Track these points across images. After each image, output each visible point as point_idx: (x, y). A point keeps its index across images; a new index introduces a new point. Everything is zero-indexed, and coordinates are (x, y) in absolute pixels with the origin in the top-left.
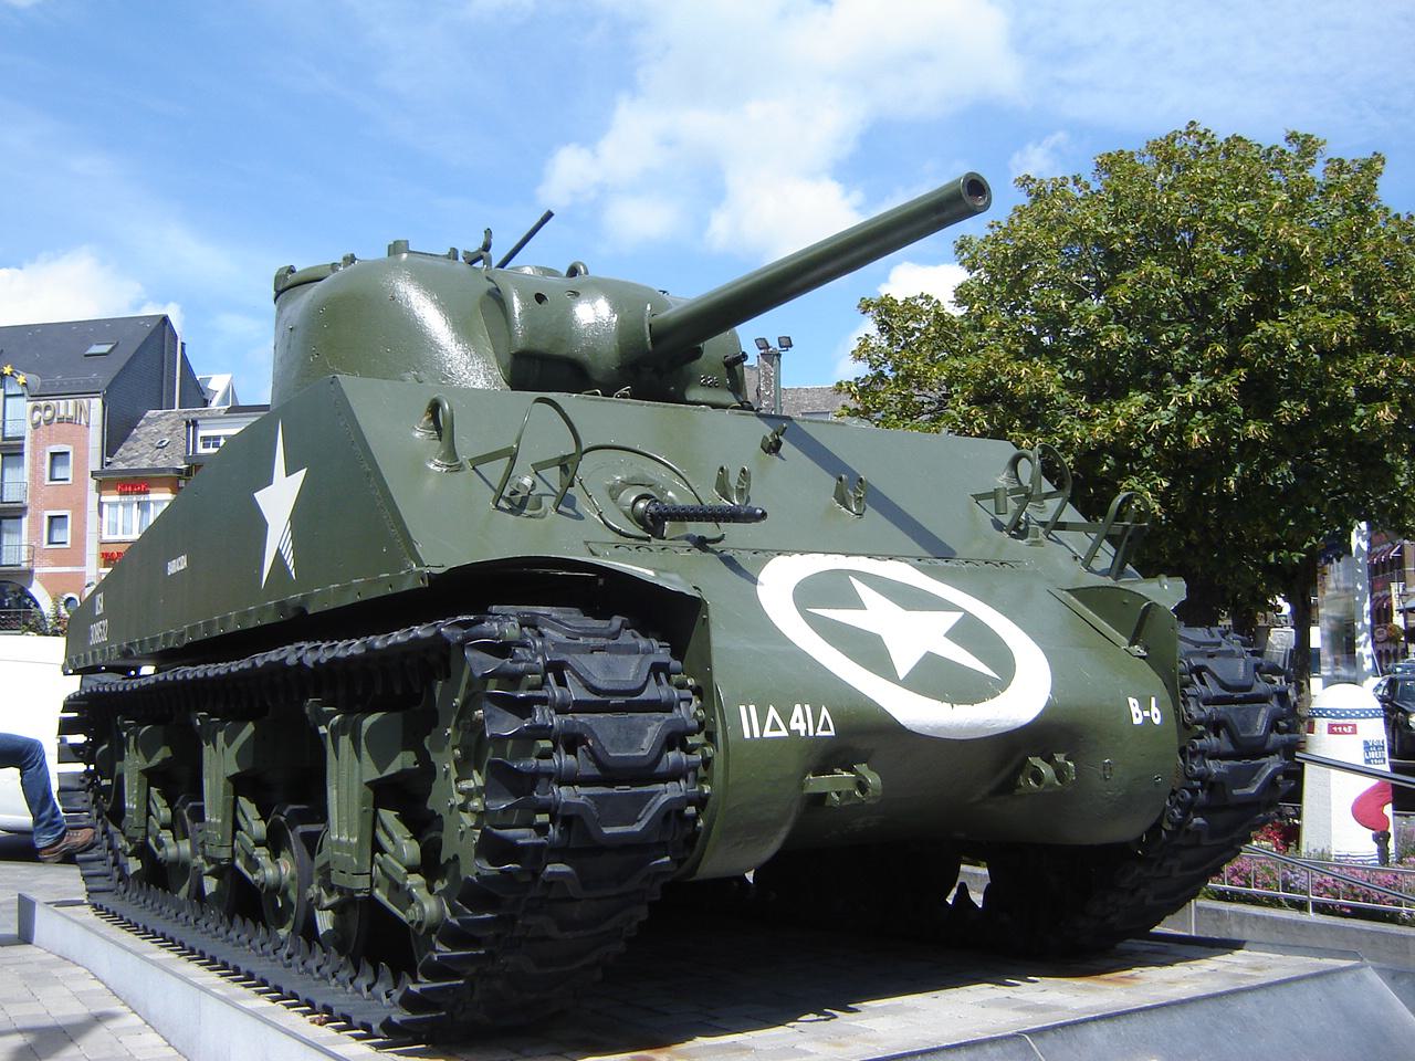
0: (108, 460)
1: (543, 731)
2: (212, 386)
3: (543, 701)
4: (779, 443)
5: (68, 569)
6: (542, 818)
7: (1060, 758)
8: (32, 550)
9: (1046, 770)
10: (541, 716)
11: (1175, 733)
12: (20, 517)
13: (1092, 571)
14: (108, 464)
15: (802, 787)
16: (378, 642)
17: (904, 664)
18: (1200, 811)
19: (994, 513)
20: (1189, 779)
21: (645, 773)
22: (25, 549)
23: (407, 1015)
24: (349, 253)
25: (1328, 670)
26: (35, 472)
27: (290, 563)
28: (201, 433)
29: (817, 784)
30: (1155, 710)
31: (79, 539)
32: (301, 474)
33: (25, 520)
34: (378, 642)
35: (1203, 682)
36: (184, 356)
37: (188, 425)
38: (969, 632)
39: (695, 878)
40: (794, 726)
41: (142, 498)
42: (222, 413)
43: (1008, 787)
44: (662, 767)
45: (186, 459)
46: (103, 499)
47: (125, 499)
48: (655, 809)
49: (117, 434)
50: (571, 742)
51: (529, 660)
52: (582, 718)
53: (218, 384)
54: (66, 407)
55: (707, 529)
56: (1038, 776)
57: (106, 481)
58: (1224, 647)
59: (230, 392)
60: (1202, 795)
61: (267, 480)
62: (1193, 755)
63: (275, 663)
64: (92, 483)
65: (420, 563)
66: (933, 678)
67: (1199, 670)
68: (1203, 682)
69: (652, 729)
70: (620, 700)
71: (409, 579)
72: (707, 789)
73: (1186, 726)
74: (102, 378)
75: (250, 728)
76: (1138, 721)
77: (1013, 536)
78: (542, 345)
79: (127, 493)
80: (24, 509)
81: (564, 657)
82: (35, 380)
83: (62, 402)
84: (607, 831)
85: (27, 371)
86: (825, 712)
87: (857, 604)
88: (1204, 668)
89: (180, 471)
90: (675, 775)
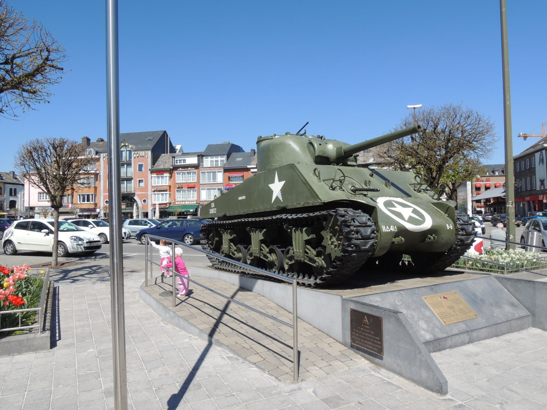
0: (153, 166)
1: (352, 231)
2: (176, 148)
3: (352, 225)
4: (373, 175)
5: (144, 193)
6: (352, 246)
7: (434, 235)
8: (135, 188)
9: (432, 237)
10: (352, 228)
11: (455, 231)
12: (131, 180)
13: (434, 199)
14: (153, 167)
15: (392, 240)
16: (311, 214)
17: (406, 218)
18: (459, 246)
19: (414, 187)
20: (457, 239)
21: (368, 238)
22: (133, 188)
23: (321, 282)
24: (275, 133)
25: (341, 211)
26: (135, 169)
27: (281, 199)
28: (176, 159)
29: (394, 240)
30: (451, 226)
31: (146, 185)
32: (283, 182)
33: (133, 181)
34: (311, 214)
35: (459, 221)
36: (170, 141)
37: (173, 158)
38: (415, 211)
39: (374, 256)
40: (391, 229)
41: (162, 175)
42: (180, 155)
43: (424, 240)
44: (371, 237)
45: (172, 166)
46: (152, 176)
47: (158, 176)
48: (370, 244)
49: (155, 160)
50: (357, 232)
51: (347, 218)
52: (359, 228)
53: (178, 147)
54: (142, 153)
55: (365, 193)
56: (430, 238)
57: (152, 172)
58: (463, 214)
59: (181, 149)
60: (460, 243)
61: (273, 182)
62: (458, 235)
63: (295, 219)
64: (149, 172)
65: (320, 200)
66: (411, 220)
67: (458, 219)
68: (459, 221)
69: (369, 230)
70: (364, 225)
71: (317, 203)
72: (377, 241)
73: (456, 229)
74: (151, 146)
75: (265, 230)
76: (448, 228)
77: (418, 192)
78: (321, 154)
79: (158, 174)
80: (132, 178)
81: (354, 218)
82: (134, 147)
83: (141, 152)
84: (363, 248)
85: (132, 144)
86: (395, 227)
87: (395, 207)
88: (459, 218)
89: (171, 169)
90: (372, 238)
